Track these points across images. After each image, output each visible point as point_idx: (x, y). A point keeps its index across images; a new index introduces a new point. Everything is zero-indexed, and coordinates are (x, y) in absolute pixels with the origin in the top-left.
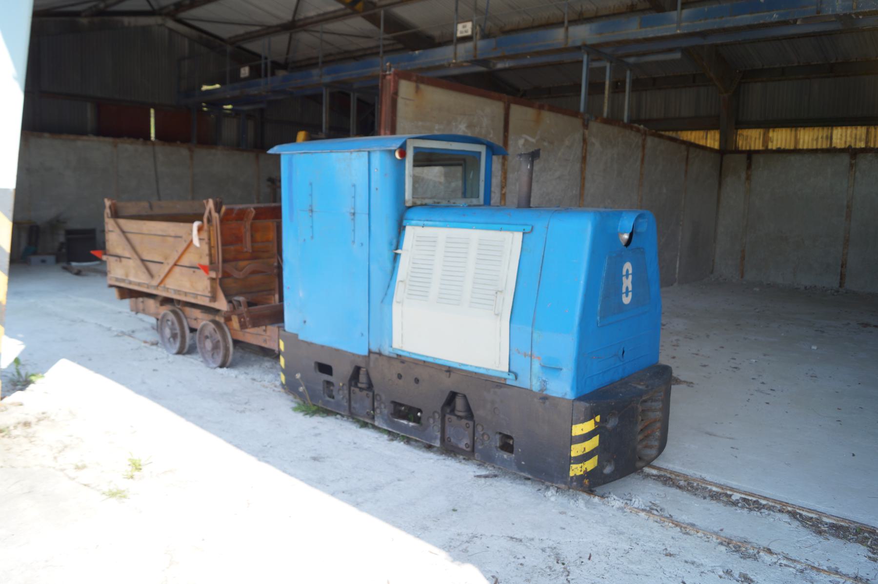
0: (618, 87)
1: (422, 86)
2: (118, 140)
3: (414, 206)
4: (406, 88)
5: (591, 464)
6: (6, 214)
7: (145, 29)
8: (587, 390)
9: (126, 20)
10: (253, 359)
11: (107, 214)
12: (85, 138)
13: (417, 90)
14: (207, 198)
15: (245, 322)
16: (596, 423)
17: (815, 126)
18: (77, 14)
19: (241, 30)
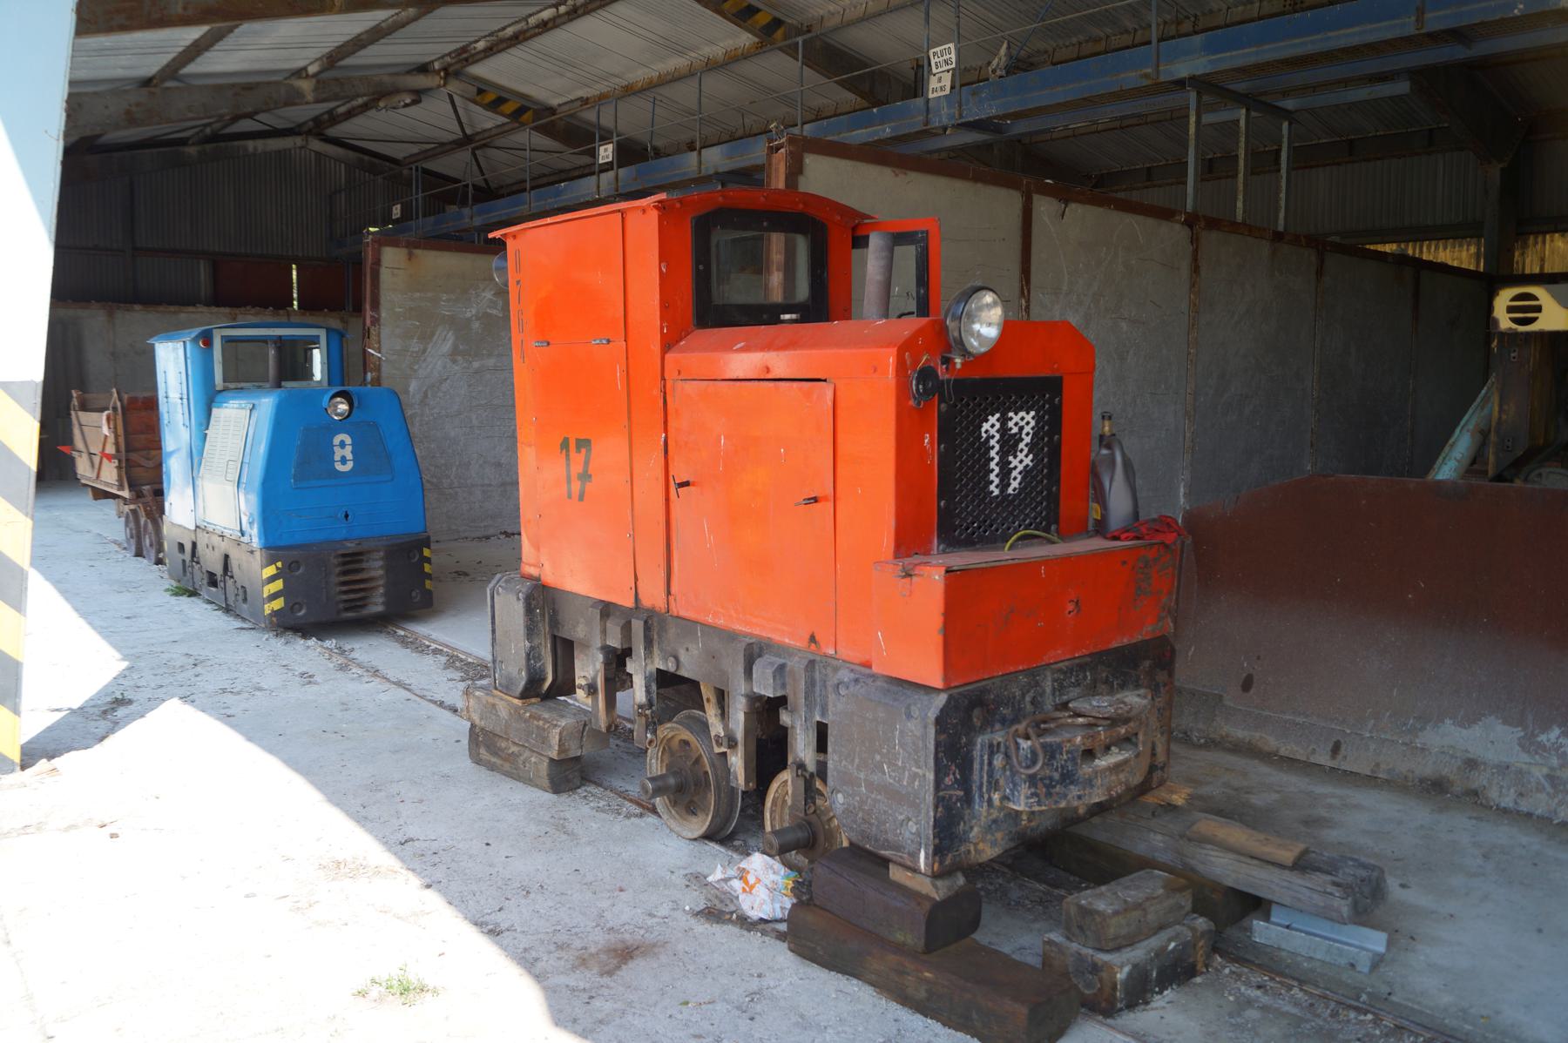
0: (1263, 162)
1: (418, 252)
2: (237, 311)
3: (225, 389)
4: (392, 257)
5: (278, 604)
6: (32, 412)
7: (280, 154)
8: (268, 545)
9: (251, 145)
10: (1506, 822)
11: (74, 405)
12: (191, 309)
13: (410, 256)
14: (112, 388)
15: (151, 511)
16: (277, 568)
17: (1464, 237)
18: (183, 142)
19: (415, 149)
